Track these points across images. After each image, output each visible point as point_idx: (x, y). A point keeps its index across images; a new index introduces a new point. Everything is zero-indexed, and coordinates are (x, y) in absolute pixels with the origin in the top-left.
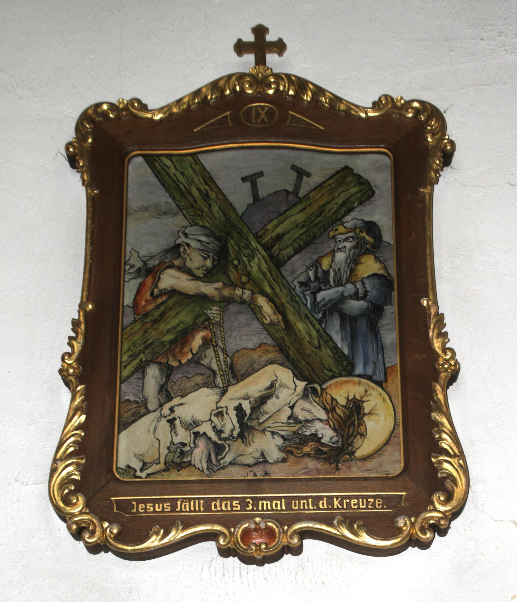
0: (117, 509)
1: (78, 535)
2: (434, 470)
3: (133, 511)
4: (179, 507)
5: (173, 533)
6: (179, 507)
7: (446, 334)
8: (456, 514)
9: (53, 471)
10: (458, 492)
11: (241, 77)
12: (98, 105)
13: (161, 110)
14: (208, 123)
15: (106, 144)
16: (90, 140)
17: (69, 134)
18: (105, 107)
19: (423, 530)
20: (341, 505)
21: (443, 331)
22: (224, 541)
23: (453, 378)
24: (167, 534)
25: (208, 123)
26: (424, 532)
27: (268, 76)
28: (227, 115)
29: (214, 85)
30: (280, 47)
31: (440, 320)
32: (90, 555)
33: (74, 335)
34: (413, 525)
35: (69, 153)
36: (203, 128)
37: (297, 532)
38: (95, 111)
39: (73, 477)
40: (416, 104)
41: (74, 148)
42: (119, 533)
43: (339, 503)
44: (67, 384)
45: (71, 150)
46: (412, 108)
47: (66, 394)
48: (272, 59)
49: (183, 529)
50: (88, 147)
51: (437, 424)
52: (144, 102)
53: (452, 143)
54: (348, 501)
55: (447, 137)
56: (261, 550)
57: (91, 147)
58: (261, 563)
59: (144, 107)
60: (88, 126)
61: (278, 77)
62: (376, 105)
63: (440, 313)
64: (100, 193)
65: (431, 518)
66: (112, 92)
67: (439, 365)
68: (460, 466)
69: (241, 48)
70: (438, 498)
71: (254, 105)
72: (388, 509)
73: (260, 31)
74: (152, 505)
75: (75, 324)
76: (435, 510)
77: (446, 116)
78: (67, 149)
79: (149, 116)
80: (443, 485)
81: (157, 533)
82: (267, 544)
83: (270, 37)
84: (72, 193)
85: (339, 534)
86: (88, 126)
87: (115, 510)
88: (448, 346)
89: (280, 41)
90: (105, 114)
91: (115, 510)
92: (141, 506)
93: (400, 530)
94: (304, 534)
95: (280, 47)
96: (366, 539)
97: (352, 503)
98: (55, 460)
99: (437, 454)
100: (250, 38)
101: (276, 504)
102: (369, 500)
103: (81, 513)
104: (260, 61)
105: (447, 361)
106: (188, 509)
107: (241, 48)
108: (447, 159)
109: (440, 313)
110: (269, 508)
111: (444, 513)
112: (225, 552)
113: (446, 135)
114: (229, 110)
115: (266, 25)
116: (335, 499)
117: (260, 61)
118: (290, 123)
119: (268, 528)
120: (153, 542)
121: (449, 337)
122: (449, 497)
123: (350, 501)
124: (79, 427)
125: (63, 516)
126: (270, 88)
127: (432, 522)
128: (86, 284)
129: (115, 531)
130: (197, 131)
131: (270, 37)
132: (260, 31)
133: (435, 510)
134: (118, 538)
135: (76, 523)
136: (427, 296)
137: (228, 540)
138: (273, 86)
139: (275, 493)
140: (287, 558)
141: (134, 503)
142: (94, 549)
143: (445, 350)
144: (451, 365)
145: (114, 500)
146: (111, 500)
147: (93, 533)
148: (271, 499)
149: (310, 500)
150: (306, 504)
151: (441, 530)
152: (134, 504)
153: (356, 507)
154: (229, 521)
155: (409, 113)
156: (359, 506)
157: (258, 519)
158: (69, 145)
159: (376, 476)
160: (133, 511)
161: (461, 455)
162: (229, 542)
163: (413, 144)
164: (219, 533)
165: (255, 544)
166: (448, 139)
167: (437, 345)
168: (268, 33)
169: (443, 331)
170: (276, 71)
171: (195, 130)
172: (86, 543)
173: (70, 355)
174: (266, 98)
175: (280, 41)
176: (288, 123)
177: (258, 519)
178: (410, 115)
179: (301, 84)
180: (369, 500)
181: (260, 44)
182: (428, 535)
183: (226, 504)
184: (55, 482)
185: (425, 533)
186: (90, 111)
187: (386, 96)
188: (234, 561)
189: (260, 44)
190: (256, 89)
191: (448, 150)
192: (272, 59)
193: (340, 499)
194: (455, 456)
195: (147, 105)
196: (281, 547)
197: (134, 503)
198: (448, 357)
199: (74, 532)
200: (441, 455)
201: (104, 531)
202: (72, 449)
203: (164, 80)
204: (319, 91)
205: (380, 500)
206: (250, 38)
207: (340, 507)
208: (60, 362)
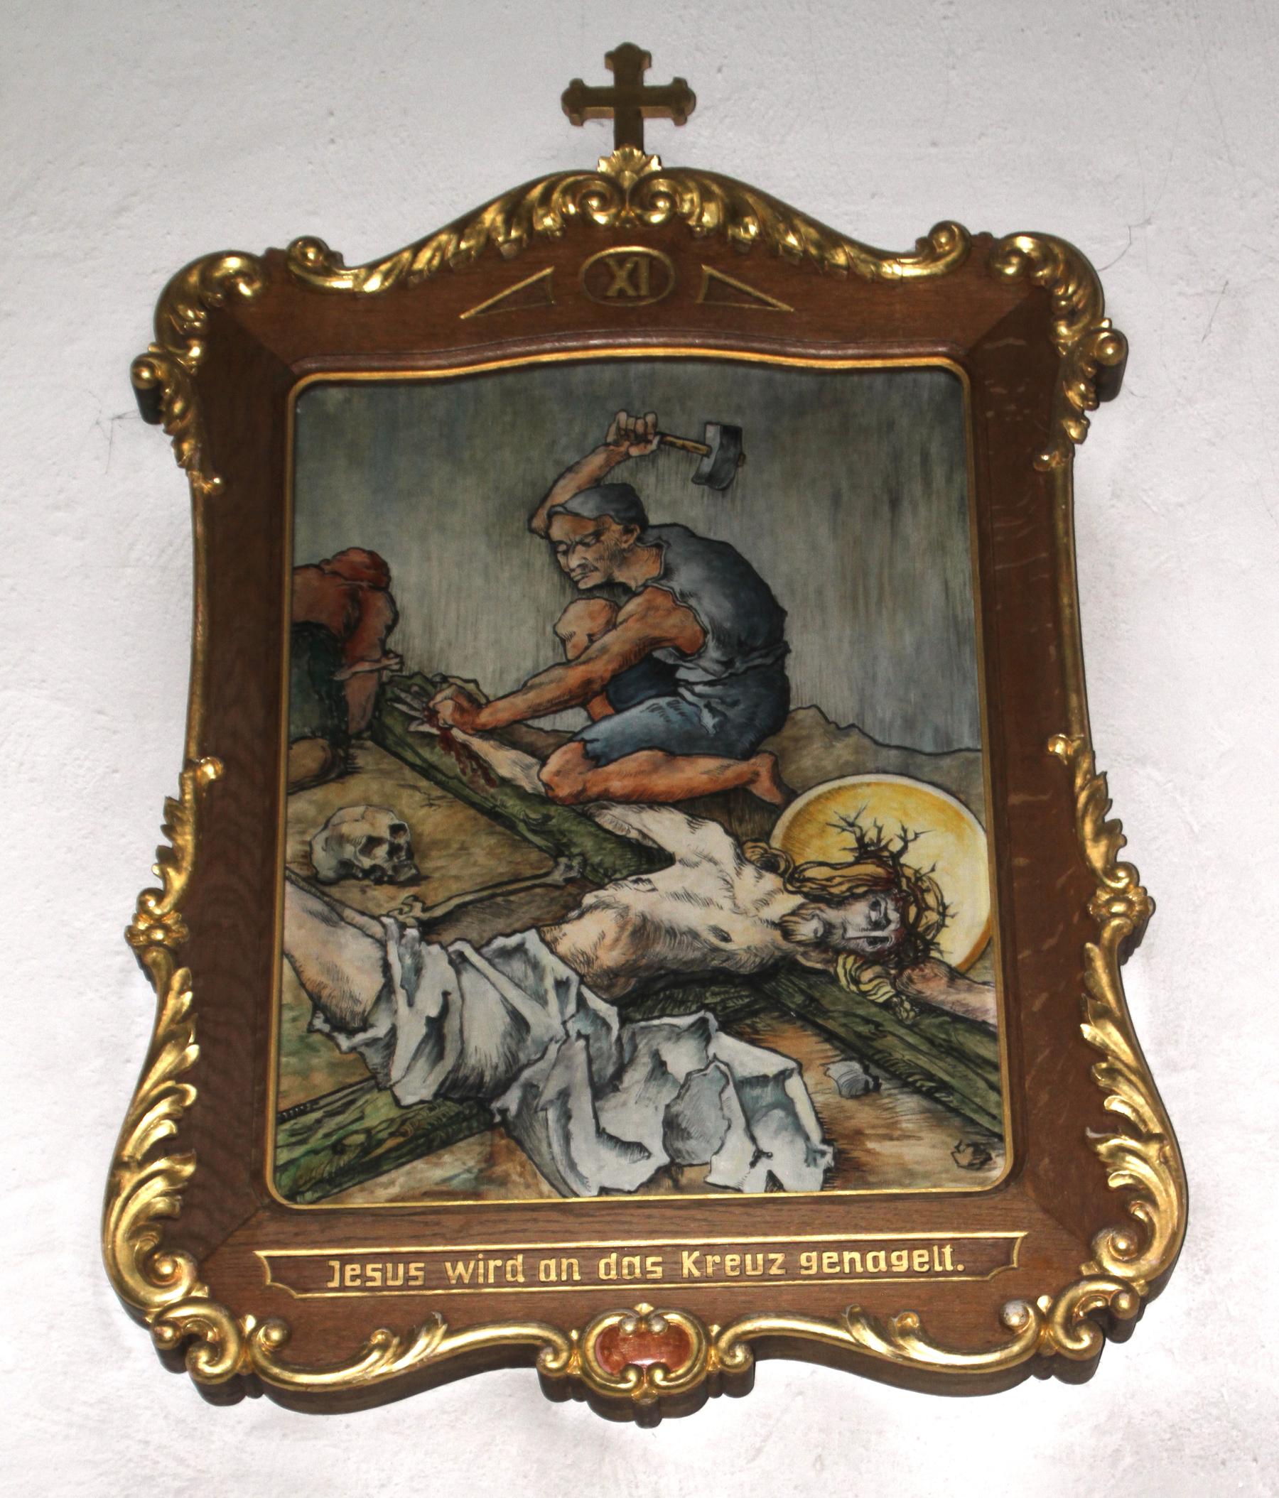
0: (273, 1280)
1: (176, 1354)
2: (1101, 1169)
3: (331, 1285)
4: (337, 1275)
5: (422, 1341)
6: (337, 1275)
7: (1117, 824)
8: (1156, 1283)
9: (113, 1190)
10: (1163, 1224)
11: (577, 185)
12: (215, 259)
13: (372, 267)
14: (500, 296)
15: (245, 366)
16: (196, 352)
17: (136, 332)
18: (233, 264)
19: (1071, 1327)
20: (699, 1269)
21: (1108, 818)
22: (555, 1359)
23: (1131, 940)
24: (407, 1342)
25: (500, 296)
26: (1072, 1333)
27: (656, 175)
28: (544, 278)
29: (516, 205)
30: (677, 100)
31: (1099, 784)
32: (214, 1408)
33: (167, 843)
34: (1045, 1319)
35: (143, 386)
36: (483, 311)
37: (745, 1338)
38: (205, 280)
39: (658, 654)
40: (1025, 244)
41: (151, 368)
42: (281, 1344)
43: (695, 1263)
44: (149, 970)
45: (146, 374)
46: (1018, 252)
47: (143, 993)
48: (656, 130)
49: (449, 1334)
50: (192, 367)
51: (1100, 1052)
52: (333, 246)
53: (1118, 339)
54: (499, 1263)
55: (1105, 324)
56: (652, 1382)
57: (198, 367)
58: (648, 1414)
59: (332, 262)
60: (190, 314)
61: (680, 177)
62: (925, 249)
63: (1098, 772)
64: (226, 481)
65: (1096, 1295)
66: (251, 226)
67: (1097, 906)
68: (1165, 1161)
69: (579, 102)
70: (1111, 1253)
71: (612, 251)
72: (968, 1275)
73: (628, 60)
74: (380, 1266)
75: (172, 809)
76: (1105, 1276)
77: (1104, 278)
78: (136, 376)
79: (343, 283)
80: (1121, 1211)
81: (384, 1347)
82: (667, 1370)
83: (655, 77)
84: (156, 486)
85: (852, 1340)
86: (190, 314)
87: (268, 1282)
88: (1123, 856)
89: (680, 84)
90: (228, 283)
91: (268, 1282)
92: (352, 1269)
93: (1011, 1334)
94: (764, 1346)
95: (677, 100)
96: (920, 1352)
97: (729, 1264)
98: (119, 1164)
99: (1104, 1132)
100: (601, 78)
101: (875, 1259)
102: (772, 1256)
103: (188, 1301)
104: (629, 135)
105: (1119, 896)
106: (553, 1277)
107: (579, 102)
108: (1106, 383)
109: (1098, 772)
110: (859, 1269)
111: (1125, 1283)
112: (558, 1388)
113: (1103, 319)
114: (548, 266)
115: (643, 46)
116: (685, 1254)
117: (629, 135)
118: (706, 299)
119: (676, 1333)
120: (375, 1366)
121: (1126, 831)
122: (1143, 1236)
123: (723, 1261)
124: (180, 1074)
125: (136, 1308)
126: (654, 208)
127: (1099, 1304)
128: (199, 675)
129: (276, 1335)
130: (467, 319)
131: (655, 77)
132: (628, 60)
133: (1105, 1276)
134: (277, 1354)
135: (174, 1324)
136: (1068, 732)
137: (564, 1355)
138: (661, 204)
139: (881, 1230)
140: (719, 1407)
141: (336, 1264)
142: (222, 1392)
143: (1112, 866)
144: (1130, 904)
145: (268, 1258)
146: (258, 1258)
147: (217, 1351)
148: (888, 1246)
149: (948, 1250)
150: (390, 1275)
151: (1114, 1325)
152: (333, 1268)
153: (358, 1283)
154: (569, 1315)
155: (1010, 264)
156: (643, 1264)
157: (644, 1308)
158: (139, 363)
159: (956, 1190)
160: (331, 1285)
161: (1167, 1136)
162: (566, 1365)
163: (1015, 350)
164: (538, 1343)
165: (639, 1369)
166: (1109, 330)
167: (1096, 854)
168: (650, 66)
169: (1108, 818)
170: (667, 164)
171: (462, 317)
172: (198, 1375)
173: (160, 895)
174: (646, 234)
175: (680, 84)
176: (700, 300)
177: (644, 1308)
178: (1010, 271)
179: (736, 197)
180: (772, 1256)
181: (629, 94)
182: (1086, 1340)
183: (875, 1259)
184: (116, 1227)
185: (1079, 1340)
186: (194, 279)
187: (943, 227)
188: (577, 1410)
189: (629, 94)
190: (619, 212)
191: (1110, 356)
192: (656, 130)
193: (696, 1254)
194: (1158, 1138)
195: (341, 256)
196: (702, 1377)
197: (336, 1264)
198: (1121, 885)
199: (169, 1346)
200: (1116, 1132)
201: (246, 1341)
202: (167, 1128)
203: (377, 208)
204: (786, 216)
205: (921, 1252)
206: (601, 78)
207: (696, 1273)
208: (132, 907)
